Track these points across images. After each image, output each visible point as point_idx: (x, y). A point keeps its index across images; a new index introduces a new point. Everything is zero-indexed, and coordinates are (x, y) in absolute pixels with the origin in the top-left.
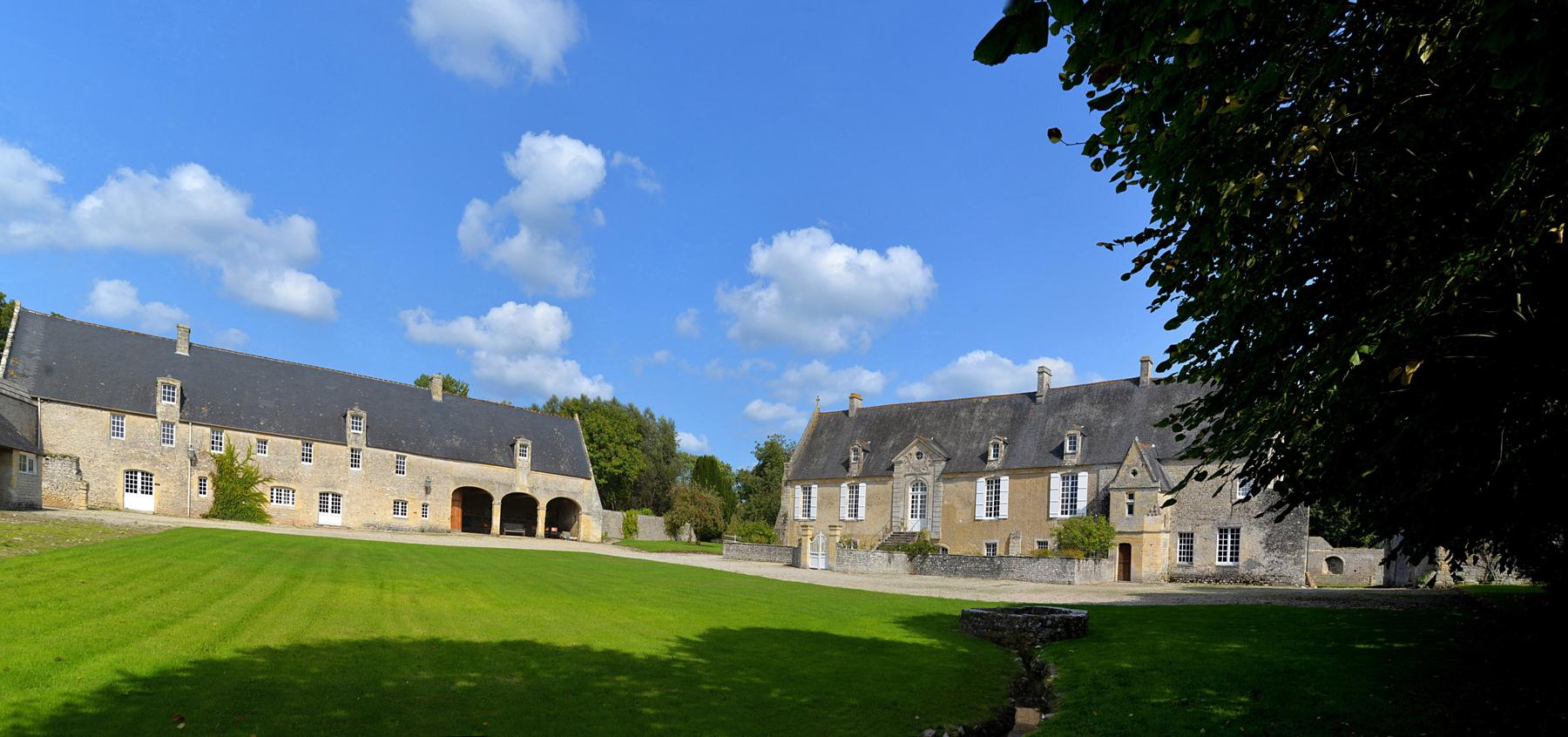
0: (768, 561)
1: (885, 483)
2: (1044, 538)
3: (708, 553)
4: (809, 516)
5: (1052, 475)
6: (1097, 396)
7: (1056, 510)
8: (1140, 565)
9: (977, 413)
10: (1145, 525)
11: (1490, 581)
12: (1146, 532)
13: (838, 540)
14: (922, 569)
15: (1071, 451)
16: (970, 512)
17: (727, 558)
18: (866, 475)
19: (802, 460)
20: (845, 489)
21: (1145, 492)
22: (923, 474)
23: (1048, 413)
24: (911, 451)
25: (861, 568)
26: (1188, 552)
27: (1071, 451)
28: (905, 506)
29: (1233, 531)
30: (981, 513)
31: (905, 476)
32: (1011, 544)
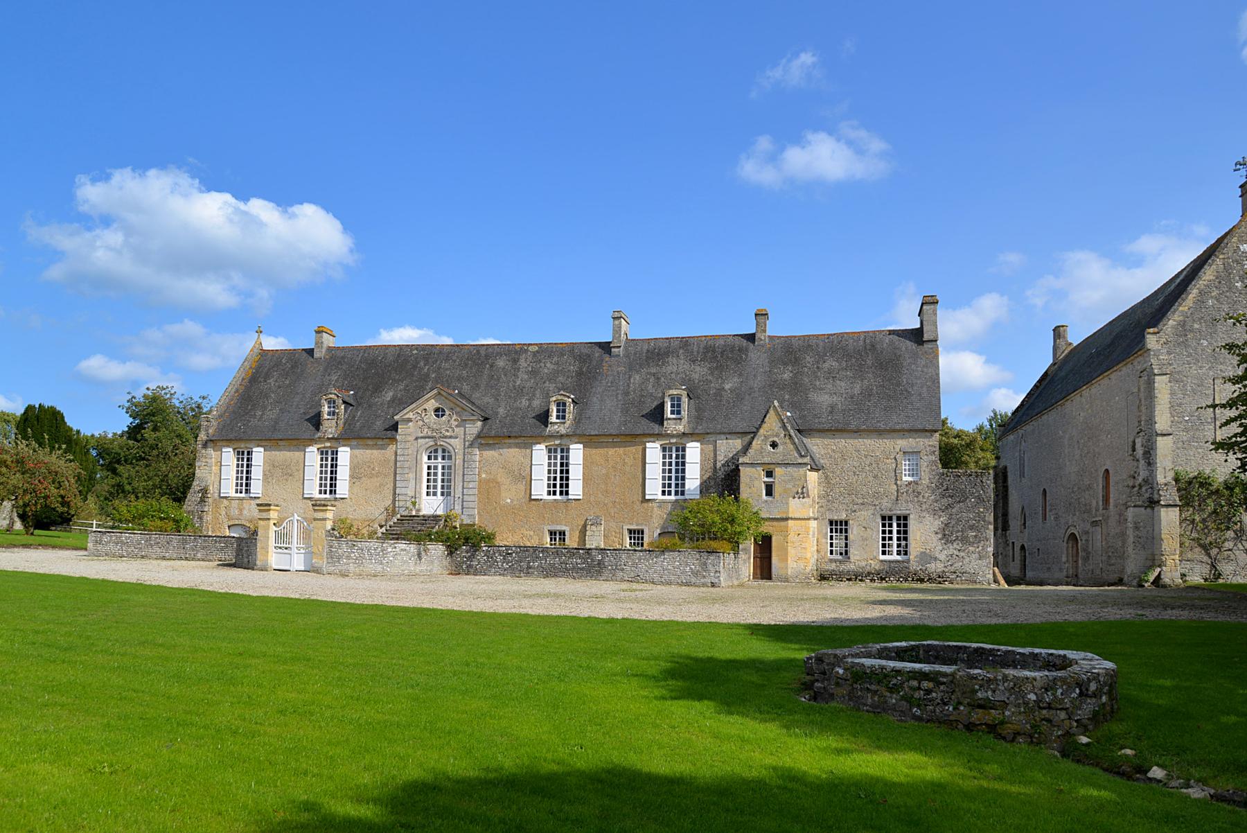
0: (181, 559)
1: (383, 447)
3: (54, 547)
4: (247, 491)
5: (648, 445)
6: (698, 353)
7: (654, 488)
8: (784, 559)
9: (523, 363)
10: (790, 509)
11: (1217, 579)
12: (792, 519)
13: (329, 525)
14: (469, 566)
15: (674, 416)
16: (523, 488)
17: (97, 555)
18: (349, 435)
19: (234, 412)
20: (313, 456)
21: (790, 469)
22: (446, 437)
23: (631, 368)
24: (426, 406)
25: (371, 567)
26: (638, 537)
27: (674, 416)
28: (417, 479)
29: (899, 518)
30: (540, 489)
31: (417, 439)
32: (588, 533)
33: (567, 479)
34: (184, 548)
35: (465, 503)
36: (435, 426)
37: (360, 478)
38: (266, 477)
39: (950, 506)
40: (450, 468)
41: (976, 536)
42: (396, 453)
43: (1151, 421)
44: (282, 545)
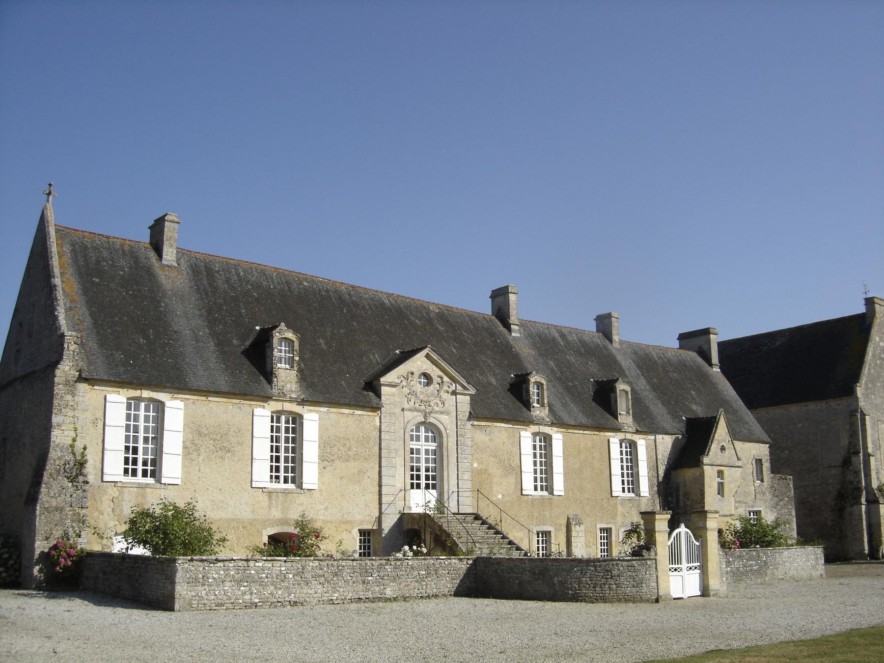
22: (437, 412)
33: (128, 428)
36: (422, 397)
38: (189, 450)
39: (777, 504)
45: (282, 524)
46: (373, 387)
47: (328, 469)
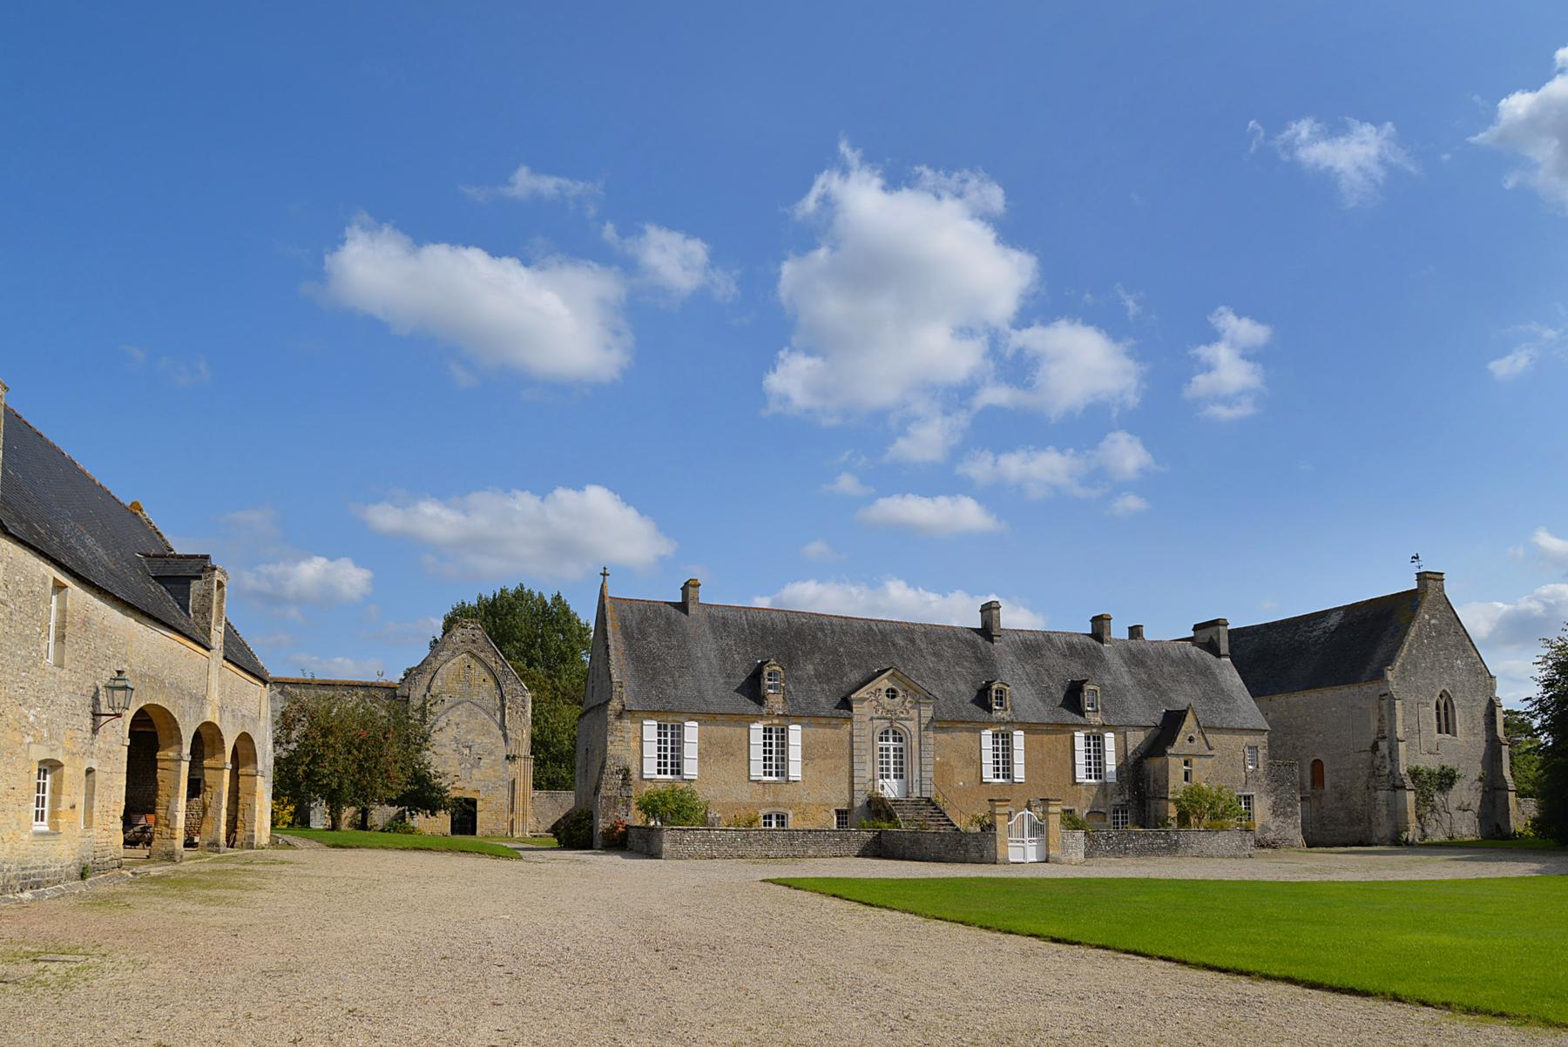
1: (836, 727)
2: (1070, 805)
16: (974, 771)
22: (902, 719)
31: (872, 719)
34: (791, 845)
35: (923, 786)
36: (888, 708)
37: (813, 759)
38: (703, 756)
39: (1276, 789)
40: (901, 750)
41: (1291, 811)
42: (851, 735)
43: (1393, 730)
44: (1014, 839)
45: (774, 806)
46: (846, 704)
47: (810, 765)
